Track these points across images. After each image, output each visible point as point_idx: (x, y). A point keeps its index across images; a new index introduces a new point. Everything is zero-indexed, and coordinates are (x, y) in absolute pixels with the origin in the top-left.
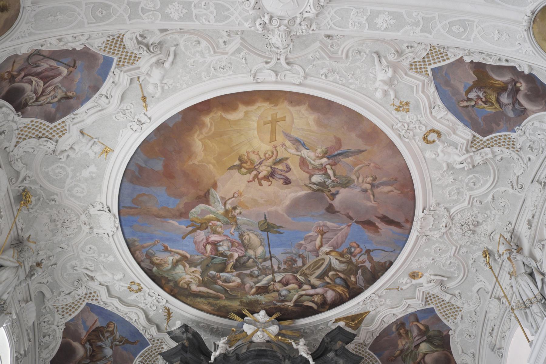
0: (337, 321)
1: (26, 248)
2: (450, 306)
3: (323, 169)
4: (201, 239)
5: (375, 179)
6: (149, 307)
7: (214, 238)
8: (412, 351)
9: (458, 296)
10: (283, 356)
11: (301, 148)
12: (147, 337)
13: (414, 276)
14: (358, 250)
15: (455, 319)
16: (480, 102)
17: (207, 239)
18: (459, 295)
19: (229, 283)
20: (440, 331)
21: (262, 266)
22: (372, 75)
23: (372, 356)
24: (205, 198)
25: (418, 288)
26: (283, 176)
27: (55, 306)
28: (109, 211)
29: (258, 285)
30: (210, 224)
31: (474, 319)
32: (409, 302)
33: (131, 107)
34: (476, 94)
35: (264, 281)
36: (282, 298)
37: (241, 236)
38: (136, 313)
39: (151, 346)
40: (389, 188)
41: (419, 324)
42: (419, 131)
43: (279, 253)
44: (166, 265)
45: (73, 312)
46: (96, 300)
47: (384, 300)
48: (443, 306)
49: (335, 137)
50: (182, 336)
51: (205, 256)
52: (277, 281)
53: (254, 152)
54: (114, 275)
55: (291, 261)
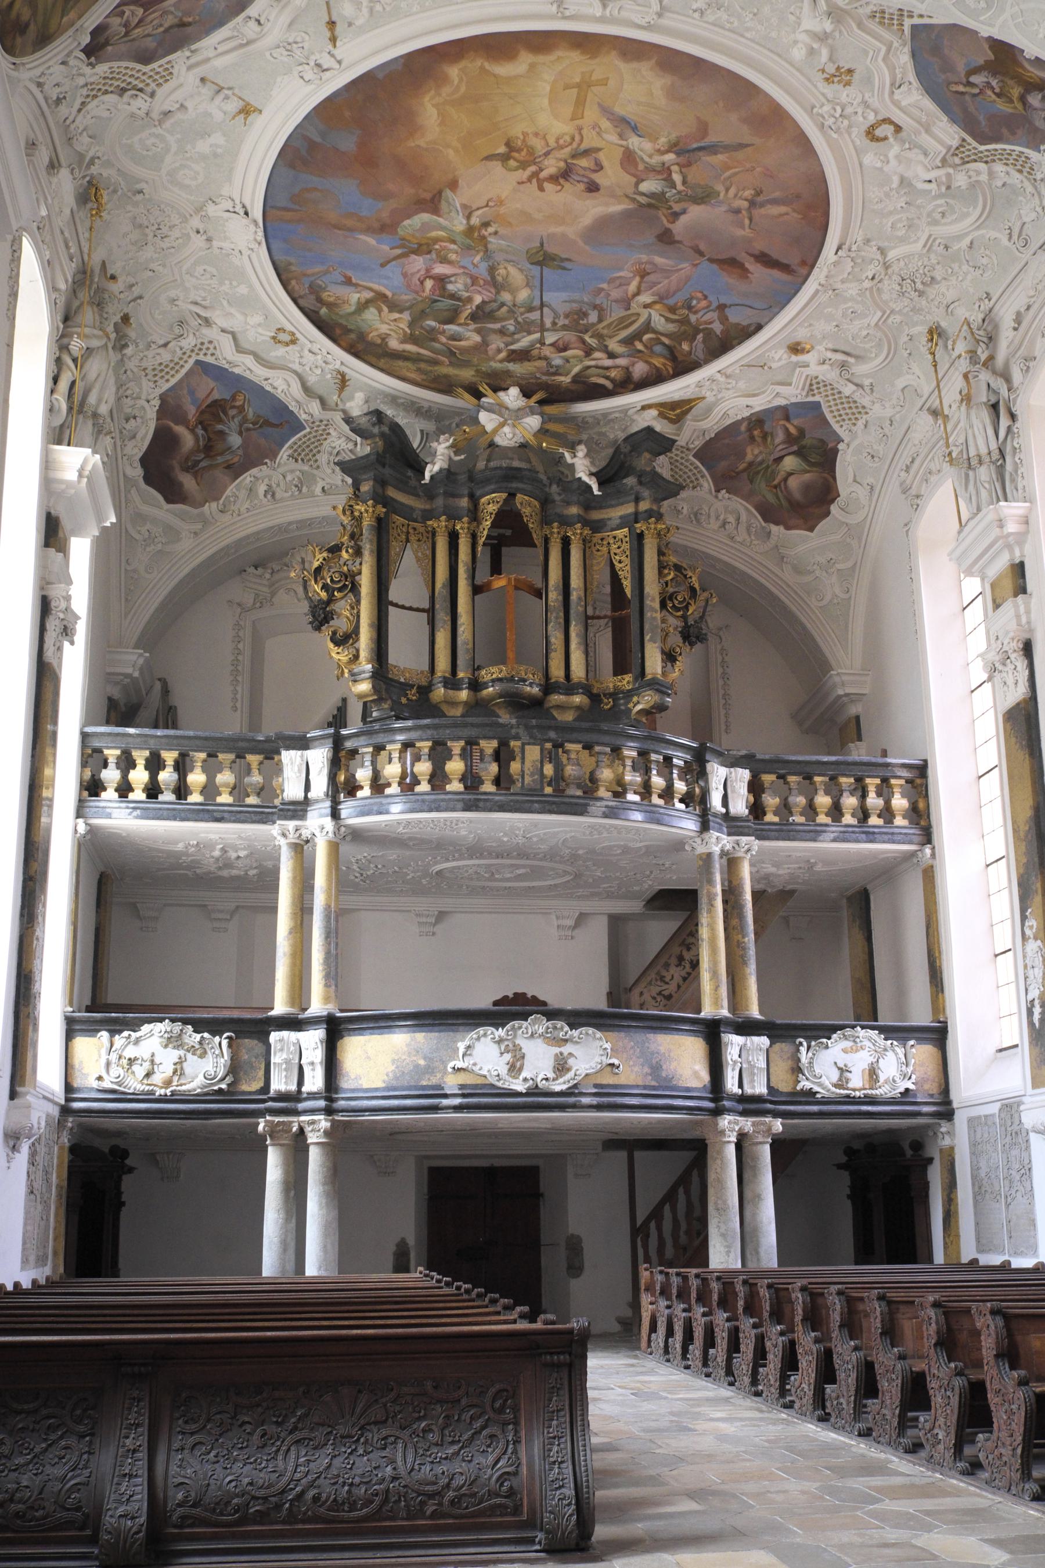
0: (644, 408)
1: (106, 296)
2: (849, 402)
3: (664, 171)
4: (415, 270)
5: (759, 193)
7: (440, 269)
8: (768, 467)
9: (867, 389)
10: (548, 478)
11: (629, 133)
12: (303, 417)
13: (797, 350)
14: (704, 303)
15: (854, 424)
16: (989, 92)
17: (428, 271)
20: (822, 441)
22: (792, 18)
23: (696, 468)
24: (433, 204)
25: (798, 369)
26: (587, 177)
28: (246, 213)
29: (512, 347)
30: (437, 247)
31: (886, 431)
33: (303, 38)
34: (985, 80)
35: (524, 342)
36: (552, 370)
37: (492, 270)
39: (308, 430)
40: (783, 209)
41: (788, 425)
42: (861, 119)
43: (558, 300)
45: (173, 376)
46: (212, 355)
48: (838, 401)
49: (698, 118)
52: (547, 343)
53: (536, 135)
54: (246, 315)
55: (577, 314)
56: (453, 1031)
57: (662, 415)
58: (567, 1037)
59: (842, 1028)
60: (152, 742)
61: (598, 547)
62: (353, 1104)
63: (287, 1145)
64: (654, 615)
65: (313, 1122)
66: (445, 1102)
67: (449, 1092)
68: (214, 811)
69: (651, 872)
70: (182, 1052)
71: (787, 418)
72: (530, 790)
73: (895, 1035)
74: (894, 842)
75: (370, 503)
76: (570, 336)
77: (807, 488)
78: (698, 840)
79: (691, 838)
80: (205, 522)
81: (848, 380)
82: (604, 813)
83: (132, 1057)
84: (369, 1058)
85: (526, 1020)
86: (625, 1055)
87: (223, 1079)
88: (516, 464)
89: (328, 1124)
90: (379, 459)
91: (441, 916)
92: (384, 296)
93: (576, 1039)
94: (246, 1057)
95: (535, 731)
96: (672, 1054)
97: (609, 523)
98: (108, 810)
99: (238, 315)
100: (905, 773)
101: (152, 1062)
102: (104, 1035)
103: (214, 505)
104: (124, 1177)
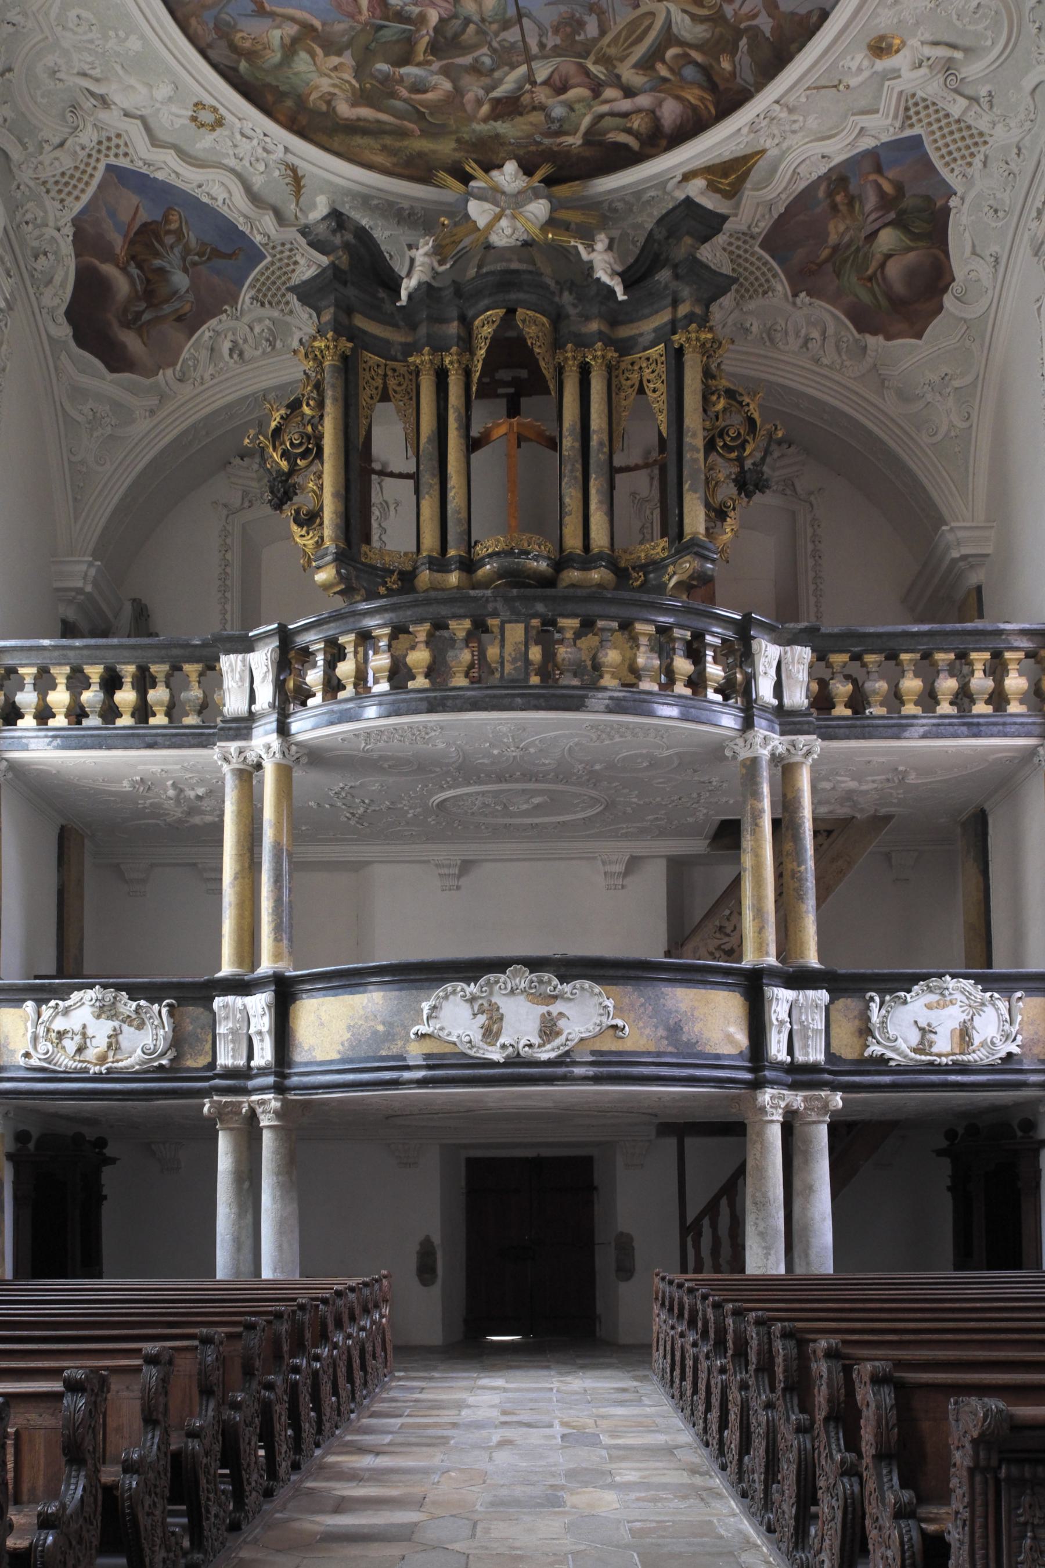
0: (687, 177)
2: (960, 130)
6: (248, 164)
8: (858, 250)
10: (557, 283)
12: (258, 239)
13: (881, 49)
18: (987, 99)
19: (425, 92)
21: (499, 43)
23: (766, 263)
25: (887, 83)
27: (38, 179)
29: (495, 94)
31: (1013, 166)
32: (865, 121)
35: (509, 82)
36: (555, 127)
38: (223, 184)
39: (269, 259)
44: (268, 54)
45: (83, 191)
46: (126, 155)
47: (801, 119)
48: (946, 131)
50: (332, 238)
51: (358, 22)
52: (539, 80)
54: (150, 86)
56: (417, 989)
57: (712, 187)
58: (556, 992)
59: (925, 977)
60: (71, 654)
61: (627, 374)
62: (306, 1079)
63: (238, 1129)
64: (696, 455)
65: (263, 1103)
66: (407, 1075)
67: (411, 1063)
68: (145, 735)
69: (699, 795)
70: (116, 1024)
71: (879, 170)
72: (512, 681)
73: (996, 986)
74: (1005, 735)
75: (330, 335)
76: (567, 65)
77: (911, 274)
78: (740, 742)
79: (732, 739)
80: (163, 398)
81: (956, 91)
82: (607, 706)
83: (62, 1029)
84: (322, 1024)
85: (504, 973)
86: (632, 1015)
87: (163, 1055)
88: (515, 266)
89: (278, 1104)
90: (334, 276)
91: (466, 866)
92: (312, 28)
93: (568, 995)
94: (191, 1028)
95: (517, 604)
96: (696, 1014)
97: (641, 340)
98: (24, 741)
99: (139, 87)
100: (1025, 643)
101: (84, 1035)
102: (30, 1006)
103: (169, 372)
104: (104, 1169)
